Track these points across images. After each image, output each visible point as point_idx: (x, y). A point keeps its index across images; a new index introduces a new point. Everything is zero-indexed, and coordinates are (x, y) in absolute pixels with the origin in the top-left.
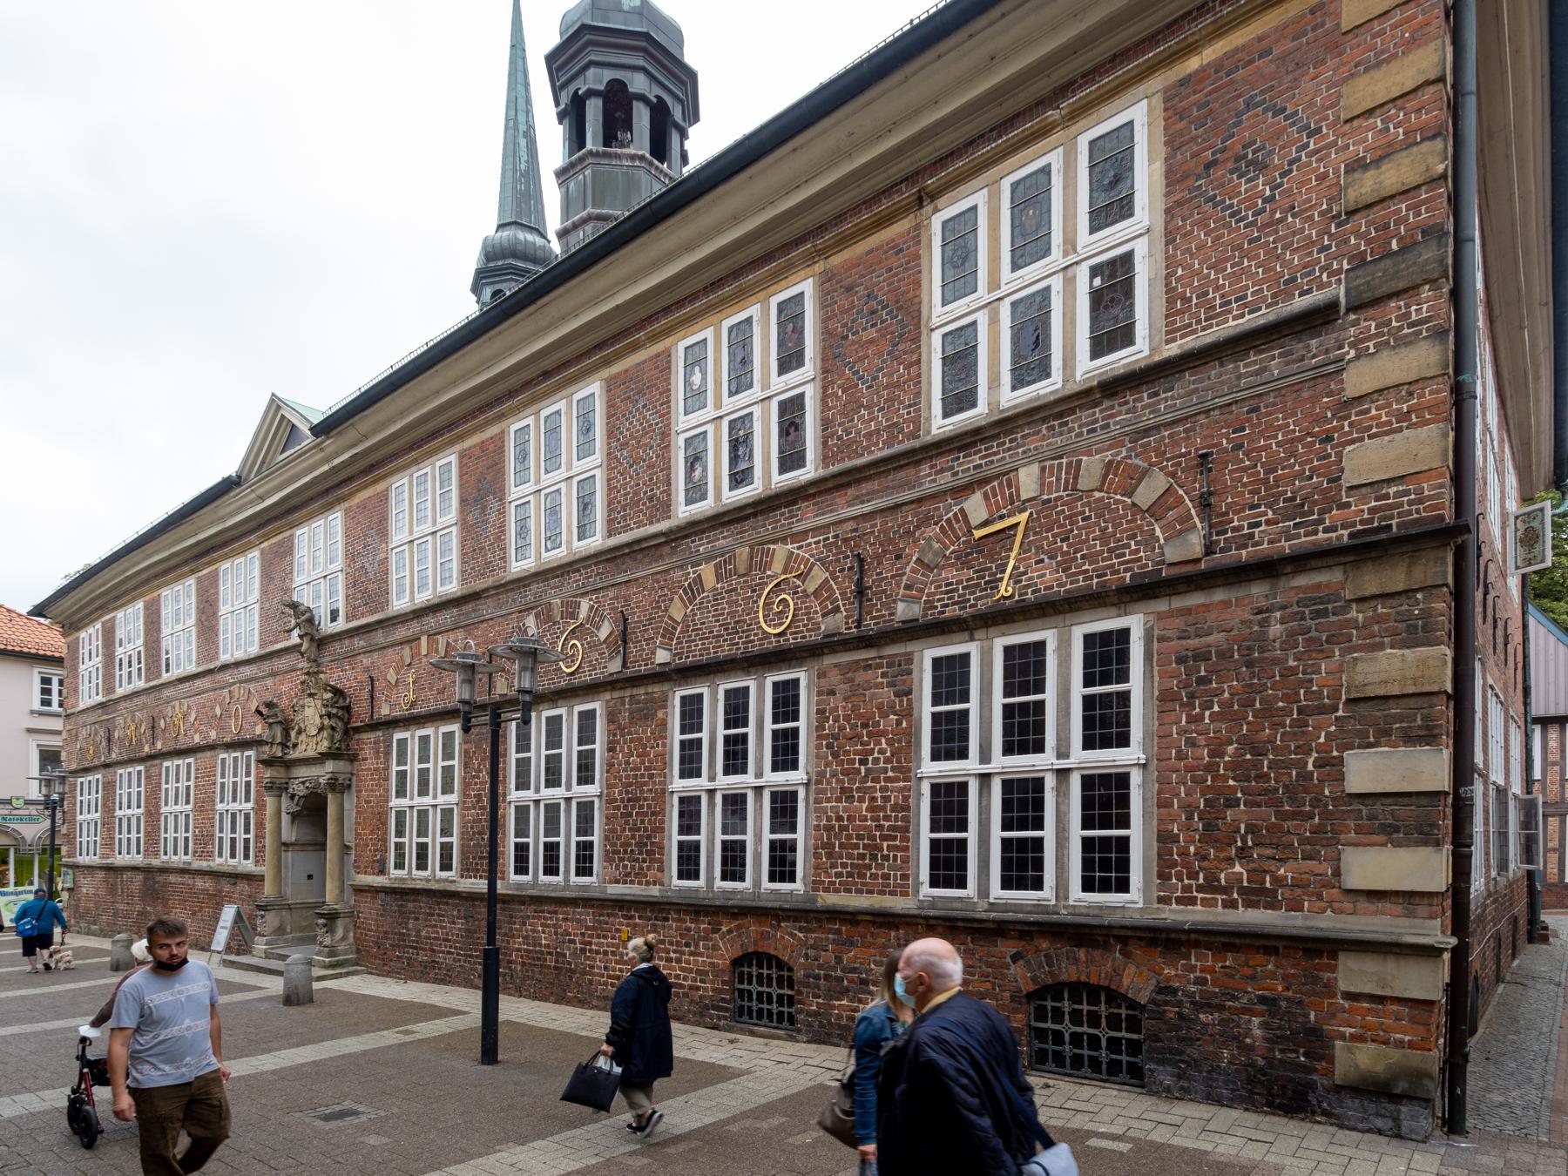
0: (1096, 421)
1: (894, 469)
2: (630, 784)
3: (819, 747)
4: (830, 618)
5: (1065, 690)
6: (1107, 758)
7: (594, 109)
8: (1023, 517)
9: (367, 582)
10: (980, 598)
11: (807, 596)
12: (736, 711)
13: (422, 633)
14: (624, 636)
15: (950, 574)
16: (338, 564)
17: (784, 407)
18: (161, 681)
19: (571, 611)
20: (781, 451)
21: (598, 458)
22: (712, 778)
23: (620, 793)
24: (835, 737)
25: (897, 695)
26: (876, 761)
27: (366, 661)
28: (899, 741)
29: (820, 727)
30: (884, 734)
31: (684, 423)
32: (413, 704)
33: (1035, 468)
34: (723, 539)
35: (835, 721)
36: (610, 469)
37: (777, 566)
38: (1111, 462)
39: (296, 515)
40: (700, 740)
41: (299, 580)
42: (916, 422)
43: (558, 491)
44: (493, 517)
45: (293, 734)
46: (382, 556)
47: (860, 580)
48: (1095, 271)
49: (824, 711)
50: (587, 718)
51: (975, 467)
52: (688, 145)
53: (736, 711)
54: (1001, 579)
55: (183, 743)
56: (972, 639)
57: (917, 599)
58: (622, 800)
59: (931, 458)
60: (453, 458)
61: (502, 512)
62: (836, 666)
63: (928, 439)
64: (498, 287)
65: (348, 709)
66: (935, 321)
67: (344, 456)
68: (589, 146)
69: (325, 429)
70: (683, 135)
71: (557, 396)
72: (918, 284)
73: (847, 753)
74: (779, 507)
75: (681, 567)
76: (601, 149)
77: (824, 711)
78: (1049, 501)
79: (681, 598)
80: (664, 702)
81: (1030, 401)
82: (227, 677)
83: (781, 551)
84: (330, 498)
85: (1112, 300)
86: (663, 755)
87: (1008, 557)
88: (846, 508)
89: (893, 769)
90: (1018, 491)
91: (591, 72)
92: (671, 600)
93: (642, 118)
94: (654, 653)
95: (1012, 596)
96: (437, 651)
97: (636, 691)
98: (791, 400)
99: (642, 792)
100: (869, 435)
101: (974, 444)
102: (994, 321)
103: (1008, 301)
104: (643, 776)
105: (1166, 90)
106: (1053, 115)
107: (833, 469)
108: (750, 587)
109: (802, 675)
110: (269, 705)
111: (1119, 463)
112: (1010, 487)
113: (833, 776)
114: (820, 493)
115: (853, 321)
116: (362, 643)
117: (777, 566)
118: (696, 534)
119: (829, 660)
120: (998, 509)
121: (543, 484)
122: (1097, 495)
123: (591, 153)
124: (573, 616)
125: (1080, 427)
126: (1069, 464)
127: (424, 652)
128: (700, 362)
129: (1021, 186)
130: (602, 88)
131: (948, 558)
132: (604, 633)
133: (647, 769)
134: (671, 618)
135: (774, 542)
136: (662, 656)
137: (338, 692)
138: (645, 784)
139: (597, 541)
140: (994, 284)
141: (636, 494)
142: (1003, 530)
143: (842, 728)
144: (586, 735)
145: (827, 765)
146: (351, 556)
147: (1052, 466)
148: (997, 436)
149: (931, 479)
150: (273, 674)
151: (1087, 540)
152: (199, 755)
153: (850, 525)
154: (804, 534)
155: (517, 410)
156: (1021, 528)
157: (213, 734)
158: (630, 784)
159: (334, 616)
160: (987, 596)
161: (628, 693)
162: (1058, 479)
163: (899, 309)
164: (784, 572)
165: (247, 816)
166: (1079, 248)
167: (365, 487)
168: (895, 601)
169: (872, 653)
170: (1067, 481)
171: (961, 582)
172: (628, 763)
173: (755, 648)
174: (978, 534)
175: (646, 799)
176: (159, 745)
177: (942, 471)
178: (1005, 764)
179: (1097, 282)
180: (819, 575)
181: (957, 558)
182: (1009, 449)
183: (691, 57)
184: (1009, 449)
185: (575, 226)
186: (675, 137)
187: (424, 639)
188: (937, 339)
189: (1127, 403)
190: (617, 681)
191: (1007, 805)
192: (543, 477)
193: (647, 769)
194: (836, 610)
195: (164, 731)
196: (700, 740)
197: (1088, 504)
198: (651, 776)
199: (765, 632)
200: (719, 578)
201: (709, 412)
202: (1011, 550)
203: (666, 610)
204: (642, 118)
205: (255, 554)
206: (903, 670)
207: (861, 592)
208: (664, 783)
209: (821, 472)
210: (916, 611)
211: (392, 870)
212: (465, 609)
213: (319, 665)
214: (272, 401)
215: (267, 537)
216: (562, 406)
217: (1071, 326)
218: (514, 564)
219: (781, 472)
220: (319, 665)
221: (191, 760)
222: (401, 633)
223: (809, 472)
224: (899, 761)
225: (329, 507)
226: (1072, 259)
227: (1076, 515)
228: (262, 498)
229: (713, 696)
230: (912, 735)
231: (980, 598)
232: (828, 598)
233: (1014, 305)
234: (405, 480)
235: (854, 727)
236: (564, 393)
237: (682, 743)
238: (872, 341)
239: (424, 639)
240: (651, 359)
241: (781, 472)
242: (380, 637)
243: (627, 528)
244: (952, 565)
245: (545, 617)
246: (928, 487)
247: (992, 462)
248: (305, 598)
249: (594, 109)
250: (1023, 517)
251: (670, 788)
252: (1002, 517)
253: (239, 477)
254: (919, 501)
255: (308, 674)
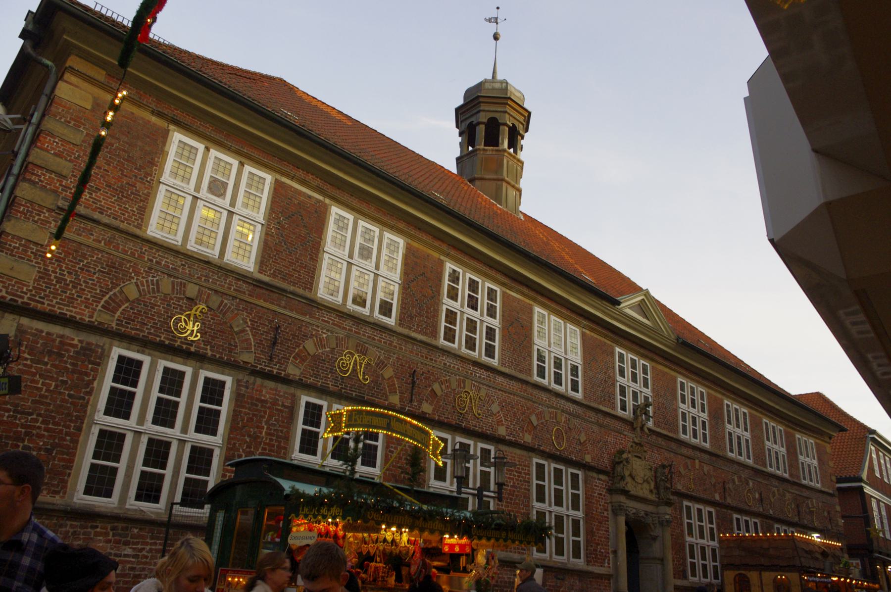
5: (189, 401)
6: (205, 439)
7: (481, 131)
70: (523, 138)
84: (651, 355)
165: (714, 550)
178: (172, 433)
191: (148, 452)
211: (690, 578)
249: (481, 131)
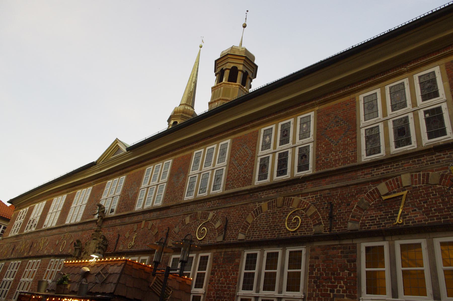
0: (434, 160)
1: (347, 172)
2: (219, 290)
3: (310, 282)
4: (317, 227)
8: (405, 193)
9: (128, 199)
10: (387, 223)
11: (307, 217)
12: (272, 260)
13: (143, 220)
14: (225, 227)
15: (373, 213)
16: (119, 193)
17: (280, 155)
18: (41, 229)
19: (205, 216)
20: (299, 164)
21: (225, 163)
22: (258, 291)
23: (214, 294)
24: (318, 278)
25: (348, 261)
26: (338, 291)
27: (119, 228)
28: (350, 283)
29: (311, 273)
30: (342, 278)
31: (261, 153)
32: (133, 247)
33: (408, 175)
34: (272, 194)
35: (318, 271)
36: (230, 167)
37: (295, 205)
38: (442, 175)
39: (110, 176)
40: (254, 273)
41: (104, 197)
42: (355, 157)
43: (208, 173)
44: (181, 181)
45: (82, 254)
46: (136, 191)
47: (331, 212)
48: (426, 112)
49: (313, 266)
50: (204, 259)
51: (381, 174)
52: (252, 83)
53: (272, 260)
54: (397, 216)
55: (40, 253)
56: (384, 240)
57: (357, 222)
58: (214, 297)
59: (362, 169)
60: (171, 161)
61: (185, 179)
62: (319, 246)
63: (360, 163)
64: (176, 120)
65: (106, 246)
66: (259, 154)
67: (128, 161)
68: (224, 81)
69: (132, 149)
70: (251, 81)
71: (214, 143)
72: (355, 114)
73: (324, 286)
74: (297, 183)
75: (254, 203)
76: (227, 82)
77: (313, 266)
78: (416, 187)
79: (252, 214)
80: (239, 256)
81: (404, 152)
82: (65, 230)
83: (296, 200)
85: (434, 121)
86: (236, 278)
87: (399, 208)
88: (326, 185)
89: (347, 296)
90: (401, 183)
91: (228, 64)
92: (248, 215)
93: (240, 76)
94: (237, 235)
95: (402, 223)
96: (147, 227)
97: (227, 250)
98: (284, 153)
99: (224, 294)
100: (335, 161)
101: (381, 165)
102: (386, 126)
103: (391, 120)
104: (225, 287)
105: (446, 64)
106: (403, 69)
107: (320, 171)
108: (282, 212)
109: (304, 250)
110: (78, 241)
111: (447, 175)
112: (397, 181)
113: (316, 296)
114: (314, 179)
115: (329, 124)
116: (119, 222)
117: (295, 205)
118: (261, 191)
119: (316, 244)
120: (393, 189)
121: (203, 171)
122: (438, 186)
123: (224, 83)
124: (206, 218)
125: (427, 161)
126: (424, 175)
127: (142, 227)
128: (270, 135)
129: (393, 88)
130: (230, 68)
131: (370, 207)
132: (217, 226)
133: (227, 284)
134: (246, 222)
135: (294, 196)
136: (241, 236)
137: (105, 239)
138: (226, 291)
139: (220, 191)
140: (294, 142)
141: (239, 176)
142: (396, 197)
143: (322, 274)
144: (203, 265)
145: (314, 291)
146: (124, 191)
147: (416, 175)
148: (390, 163)
149: (361, 177)
150: (83, 230)
151: (436, 203)
152: (43, 259)
153: (327, 191)
154: (307, 194)
155: (198, 147)
156: (404, 198)
157: (52, 251)
158: (219, 290)
159: (112, 211)
160: (390, 223)
161: (224, 250)
162: (419, 179)
163: (347, 121)
164: (298, 207)
166: (418, 105)
167: (137, 168)
168: (347, 222)
169: (337, 243)
170: (423, 180)
171: (378, 216)
172: (219, 280)
173: (282, 236)
174: (384, 198)
175: (225, 298)
176: (30, 254)
177: (367, 174)
179: (427, 115)
180: (313, 210)
181: (375, 207)
182: (396, 168)
183: (256, 62)
184: (396, 168)
185: (215, 101)
186: (249, 80)
187: (144, 222)
188: (363, 131)
189: (447, 154)
190: (221, 245)
192: (203, 168)
193: (227, 284)
194: (320, 223)
195: (34, 248)
196: (254, 273)
197: (435, 189)
198: (229, 287)
199: (287, 230)
200: (269, 208)
201: (271, 150)
202: (400, 205)
203: (245, 219)
204: (240, 76)
205: (91, 188)
206: (354, 249)
207: (331, 217)
208: (234, 291)
209: (315, 172)
210: (357, 226)
212: (162, 212)
213: (101, 228)
214: (116, 140)
215: (97, 182)
216: (214, 147)
217: (293, 161)
218: (186, 197)
219: (277, 176)
220: (101, 228)
221: (40, 260)
222: (135, 219)
223: (310, 171)
224: (350, 292)
225: (121, 174)
226: (214, 168)
227: (430, 193)
228: (101, 170)
229: (262, 255)
230: (357, 279)
231: (387, 223)
232: (316, 219)
233: (279, 154)
234: (152, 167)
235: (327, 274)
236: (204, 147)
237: (245, 274)
238: (337, 131)
239: (144, 222)
240: (251, 133)
241: (277, 176)
242: (127, 220)
243: (233, 187)
244: (373, 209)
245: (194, 217)
246: (361, 180)
247: (389, 172)
248: (102, 203)
249: (227, 73)
250: (405, 193)
251: (238, 294)
252: (395, 192)
253: (96, 162)
254: (357, 184)
255: (96, 231)
